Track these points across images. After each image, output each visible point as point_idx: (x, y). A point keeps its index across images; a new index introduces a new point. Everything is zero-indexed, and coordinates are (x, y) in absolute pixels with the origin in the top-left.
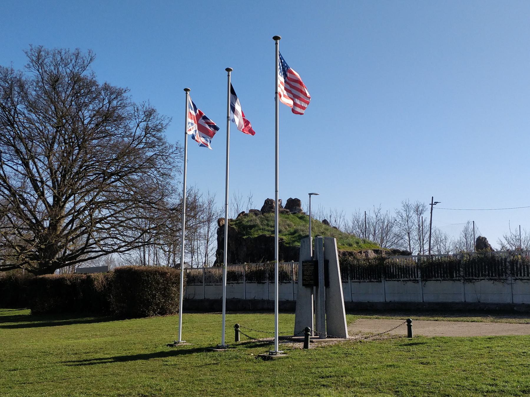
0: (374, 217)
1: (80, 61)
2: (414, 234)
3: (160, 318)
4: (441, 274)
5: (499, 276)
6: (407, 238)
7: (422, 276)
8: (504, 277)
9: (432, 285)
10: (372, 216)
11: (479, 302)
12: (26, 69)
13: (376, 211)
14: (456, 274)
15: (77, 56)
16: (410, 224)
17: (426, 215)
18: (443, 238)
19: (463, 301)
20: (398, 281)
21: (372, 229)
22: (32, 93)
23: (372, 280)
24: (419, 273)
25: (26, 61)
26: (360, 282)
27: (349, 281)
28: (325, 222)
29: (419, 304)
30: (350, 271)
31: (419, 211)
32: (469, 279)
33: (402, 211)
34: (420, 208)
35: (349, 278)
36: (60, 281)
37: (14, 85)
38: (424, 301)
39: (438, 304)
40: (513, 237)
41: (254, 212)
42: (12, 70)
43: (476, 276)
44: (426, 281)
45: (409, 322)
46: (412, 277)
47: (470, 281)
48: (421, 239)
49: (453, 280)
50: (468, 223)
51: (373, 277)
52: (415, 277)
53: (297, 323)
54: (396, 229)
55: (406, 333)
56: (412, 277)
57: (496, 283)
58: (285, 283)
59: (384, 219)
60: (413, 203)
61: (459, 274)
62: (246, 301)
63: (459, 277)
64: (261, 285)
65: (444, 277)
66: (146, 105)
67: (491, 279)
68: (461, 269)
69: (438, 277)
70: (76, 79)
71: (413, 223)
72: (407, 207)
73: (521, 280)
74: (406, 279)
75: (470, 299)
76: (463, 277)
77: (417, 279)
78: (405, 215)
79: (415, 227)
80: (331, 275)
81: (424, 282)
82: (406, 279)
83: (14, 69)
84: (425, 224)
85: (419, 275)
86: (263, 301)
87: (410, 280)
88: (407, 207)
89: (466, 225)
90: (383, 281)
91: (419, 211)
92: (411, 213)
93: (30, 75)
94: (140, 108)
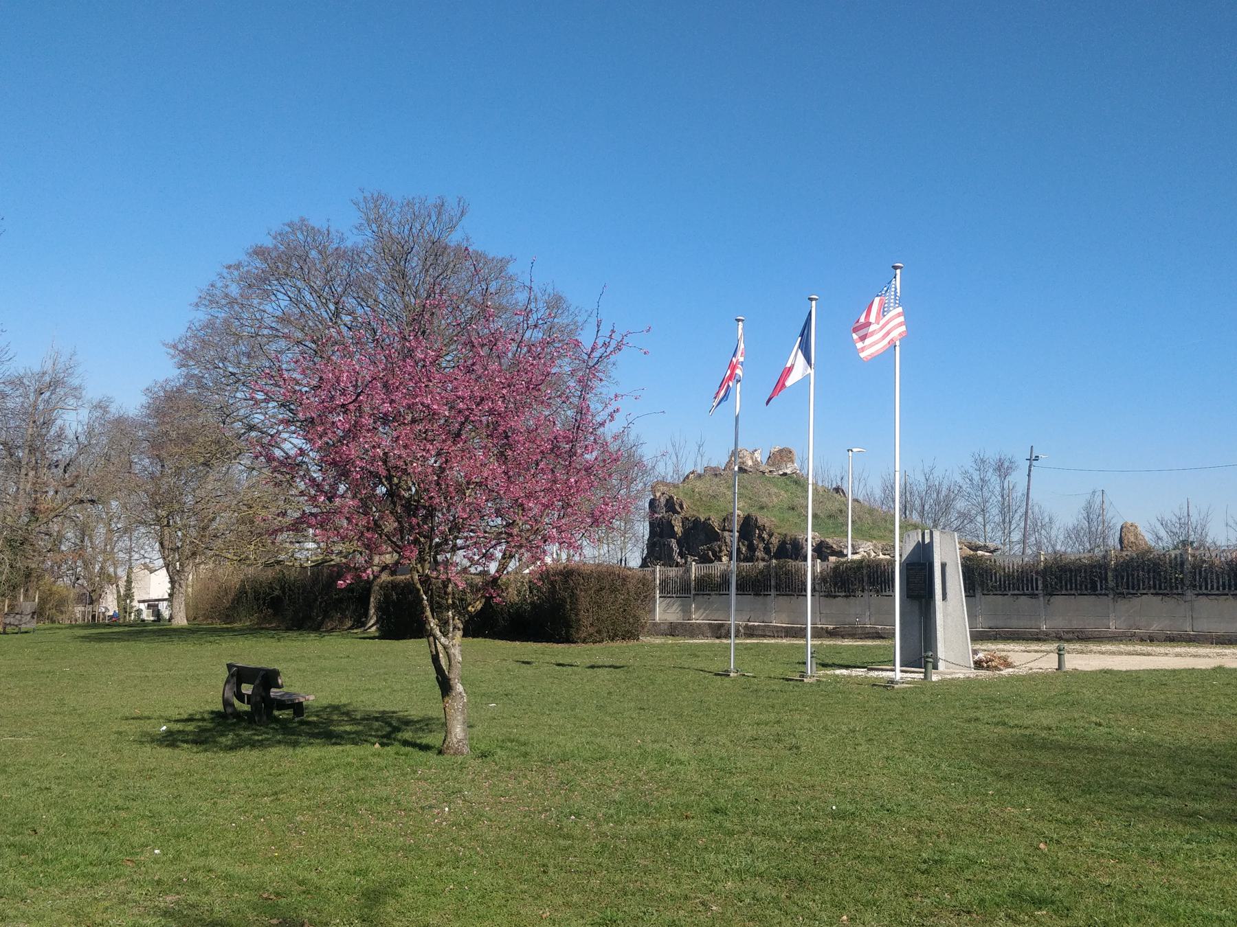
0: (923, 480)
1: (445, 217)
2: (994, 511)
5: (1171, 588)
6: (980, 519)
8: (1180, 591)
13: (927, 470)
15: (440, 207)
16: (986, 494)
17: (1018, 478)
18: (1047, 520)
21: (918, 502)
30: (980, 578)
31: (1003, 469)
33: (971, 470)
34: (1006, 464)
36: (426, 622)
40: (1174, 519)
44: (1051, 595)
48: (1006, 522)
50: (1094, 492)
54: (960, 505)
57: (1166, 599)
59: (940, 484)
60: (992, 455)
66: (550, 290)
67: (1157, 594)
70: (436, 250)
71: (993, 492)
72: (981, 463)
73: (1207, 595)
78: (976, 478)
79: (995, 499)
80: (1153, 610)
84: (1014, 495)
85: (1040, 586)
88: (981, 463)
89: (1088, 497)
90: (978, 596)
91: (1003, 469)
92: (989, 474)
94: (539, 295)
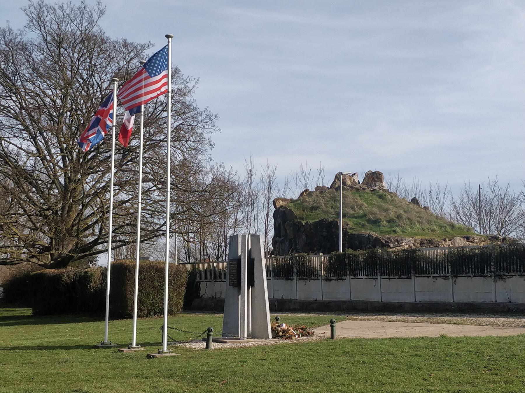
3: (500, 335)
4: (472, 270)
7: (453, 271)
9: (463, 282)
10: (487, 193)
11: (510, 302)
12: (27, 30)
14: (487, 270)
19: (494, 301)
20: (428, 277)
22: (37, 56)
23: (402, 276)
24: (449, 267)
25: (24, 20)
26: (389, 278)
27: (379, 277)
28: (414, 201)
29: (449, 304)
32: (500, 275)
35: (378, 274)
37: (17, 49)
38: (455, 301)
39: (467, 304)
41: (320, 190)
42: (10, 30)
43: (466, 273)
44: (456, 277)
45: (332, 322)
46: (442, 273)
47: (501, 277)
49: (485, 276)
51: (403, 272)
52: (445, 273)
53: (225, 324)
55: (328, 333)
56: (442, 273)
58: (313, 279)
61: (490, 269)
62: (296, 302)
63: (490, 272)
64: (289, 281)
65: (475, 272)
68: (492, 264)
69: (469, 272)
74: (436, 275)
75: (501, 299)
76: (494, 273)
77: (447, 275)
81: (454, 279)
82: (436, 275)
83: (13, 28)
85: (450, 270)
86: (290, 301)
87: (440, 276)
93: (33, 37)
